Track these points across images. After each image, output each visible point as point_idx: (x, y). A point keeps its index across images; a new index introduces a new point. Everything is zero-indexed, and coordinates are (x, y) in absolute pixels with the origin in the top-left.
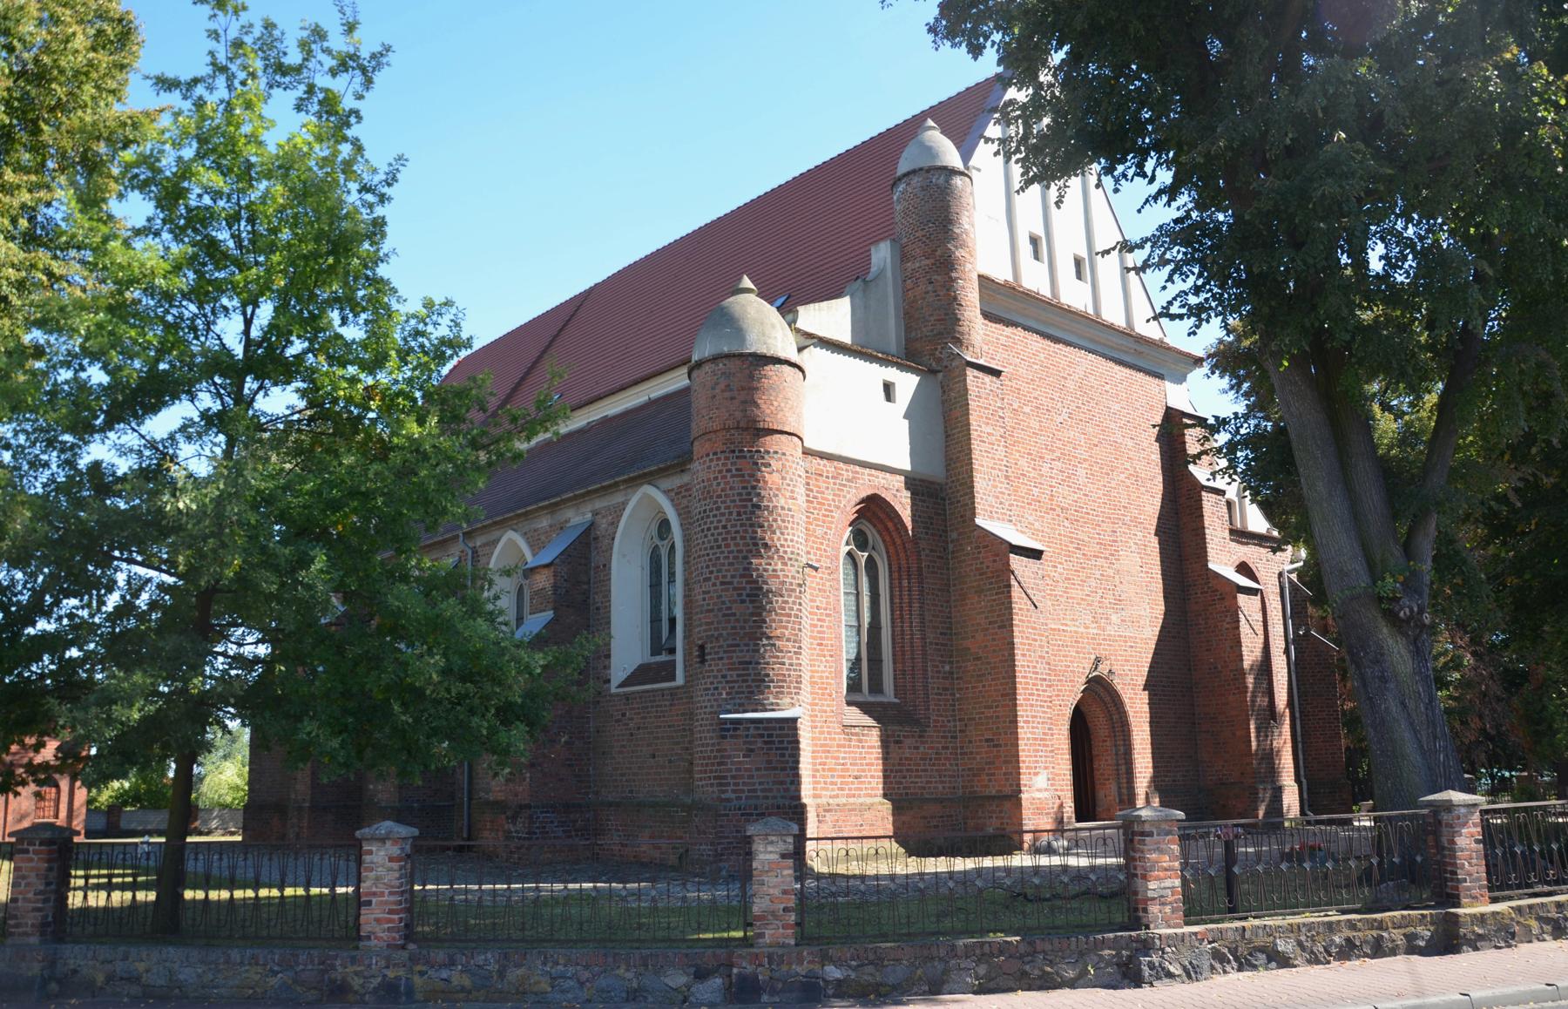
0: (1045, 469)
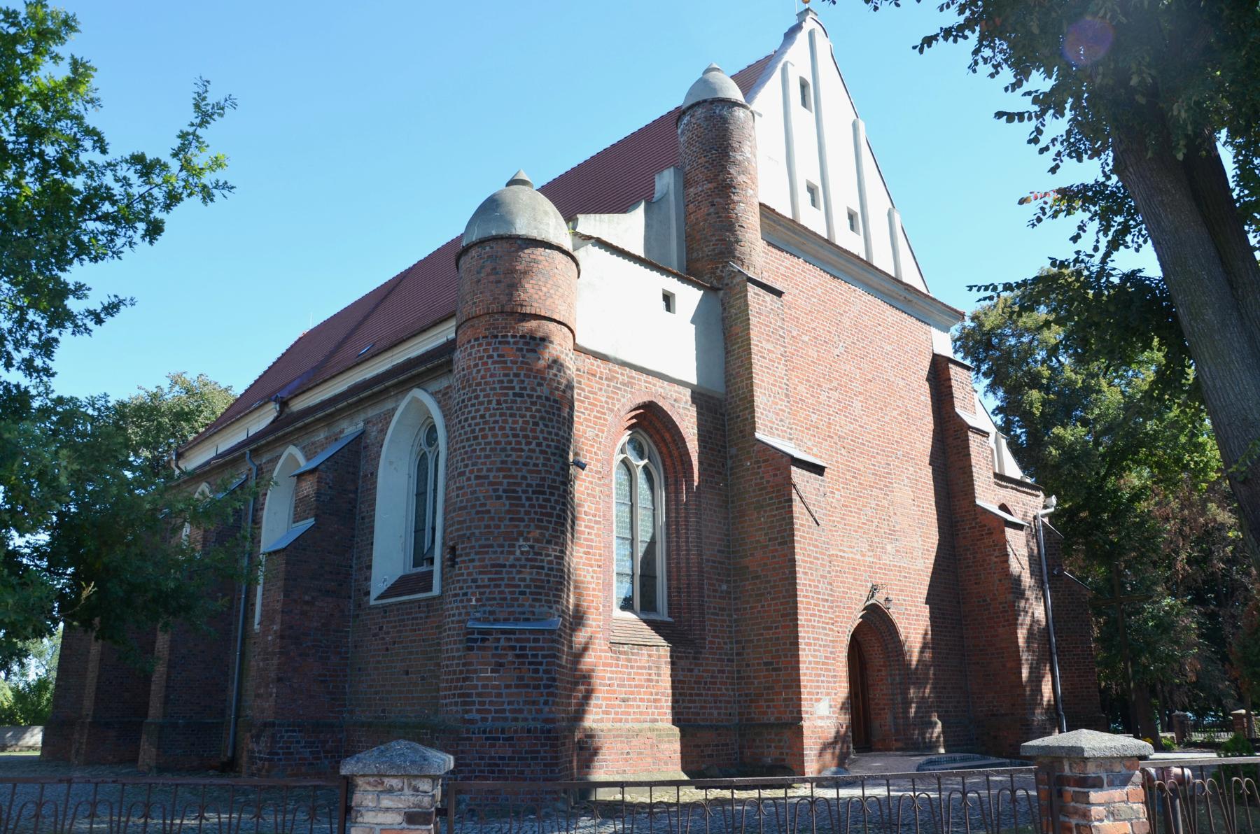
0: (823, 398)
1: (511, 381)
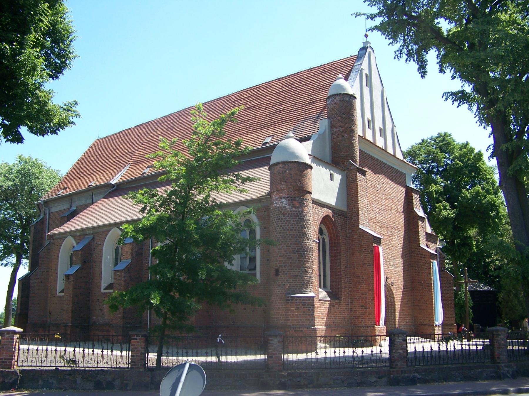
1: (297, 214)
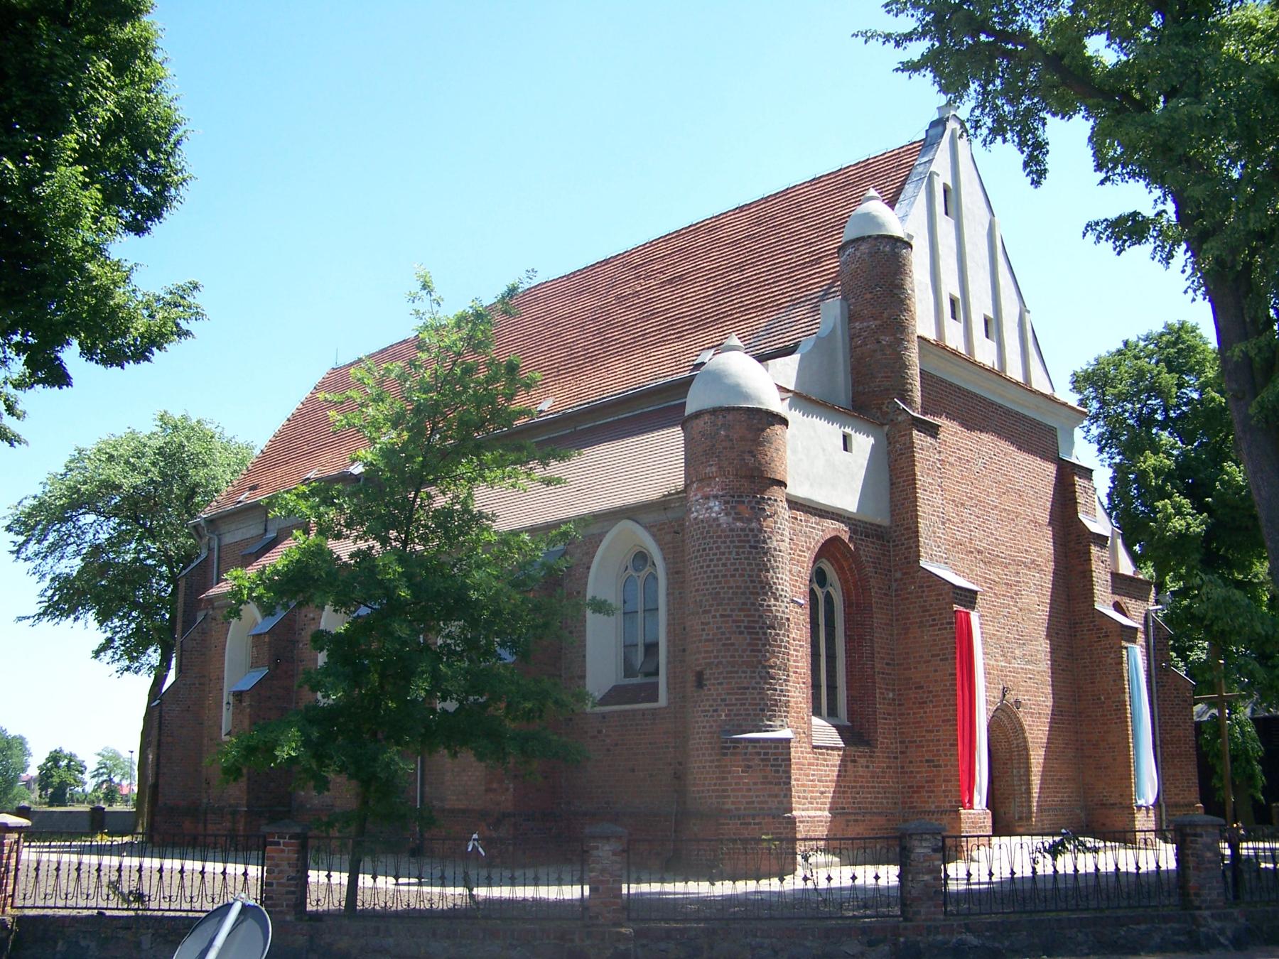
1: (747, 535)
